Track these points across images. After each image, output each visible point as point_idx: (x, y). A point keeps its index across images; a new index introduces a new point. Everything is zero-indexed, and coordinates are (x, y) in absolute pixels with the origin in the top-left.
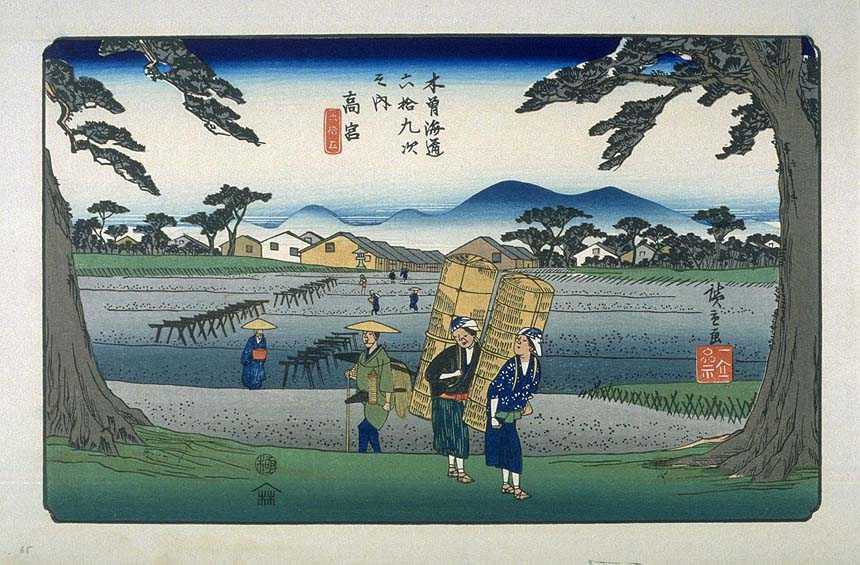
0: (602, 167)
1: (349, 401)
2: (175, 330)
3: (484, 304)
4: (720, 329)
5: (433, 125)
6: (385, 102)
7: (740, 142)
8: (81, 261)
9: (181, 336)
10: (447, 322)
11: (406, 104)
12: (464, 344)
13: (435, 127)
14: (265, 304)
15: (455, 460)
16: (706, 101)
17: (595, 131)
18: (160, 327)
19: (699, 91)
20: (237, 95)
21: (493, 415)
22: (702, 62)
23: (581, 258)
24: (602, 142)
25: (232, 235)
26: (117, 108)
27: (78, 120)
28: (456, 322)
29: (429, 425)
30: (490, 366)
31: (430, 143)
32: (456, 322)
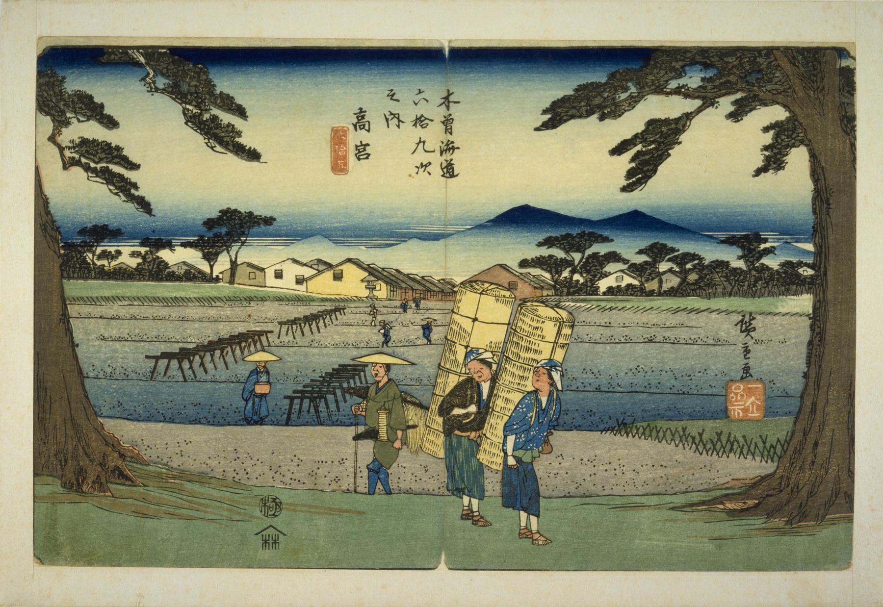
0: (624, 189)
1: (357, 438)
2: (174, 363)
3: (498, 335)
4: (751, 362)
5: (447, 145)
6: (398, 118)
7: (774, 160)
8: (74, 287)
9: (181, 367)
10: (461, 352)
11: (420, 121)
12: (480, 377)
13: (449, 147)
14: (269, 335)
15: (470, 501)
16: (735, 116)
17: (617, 151)
18: (157, 358)
19: (726, 104)
20: (241, 112)
21: (510, 452)
22: (736, 73)
23: (603, 285)
24: (624, 162)
25: (234, 265)
26: (111, 123)
27: (69, 135)
28: (470, 352)
29: (443, 465)
30: (507, 400)
31: (444, 165)
32: (470, 352)
